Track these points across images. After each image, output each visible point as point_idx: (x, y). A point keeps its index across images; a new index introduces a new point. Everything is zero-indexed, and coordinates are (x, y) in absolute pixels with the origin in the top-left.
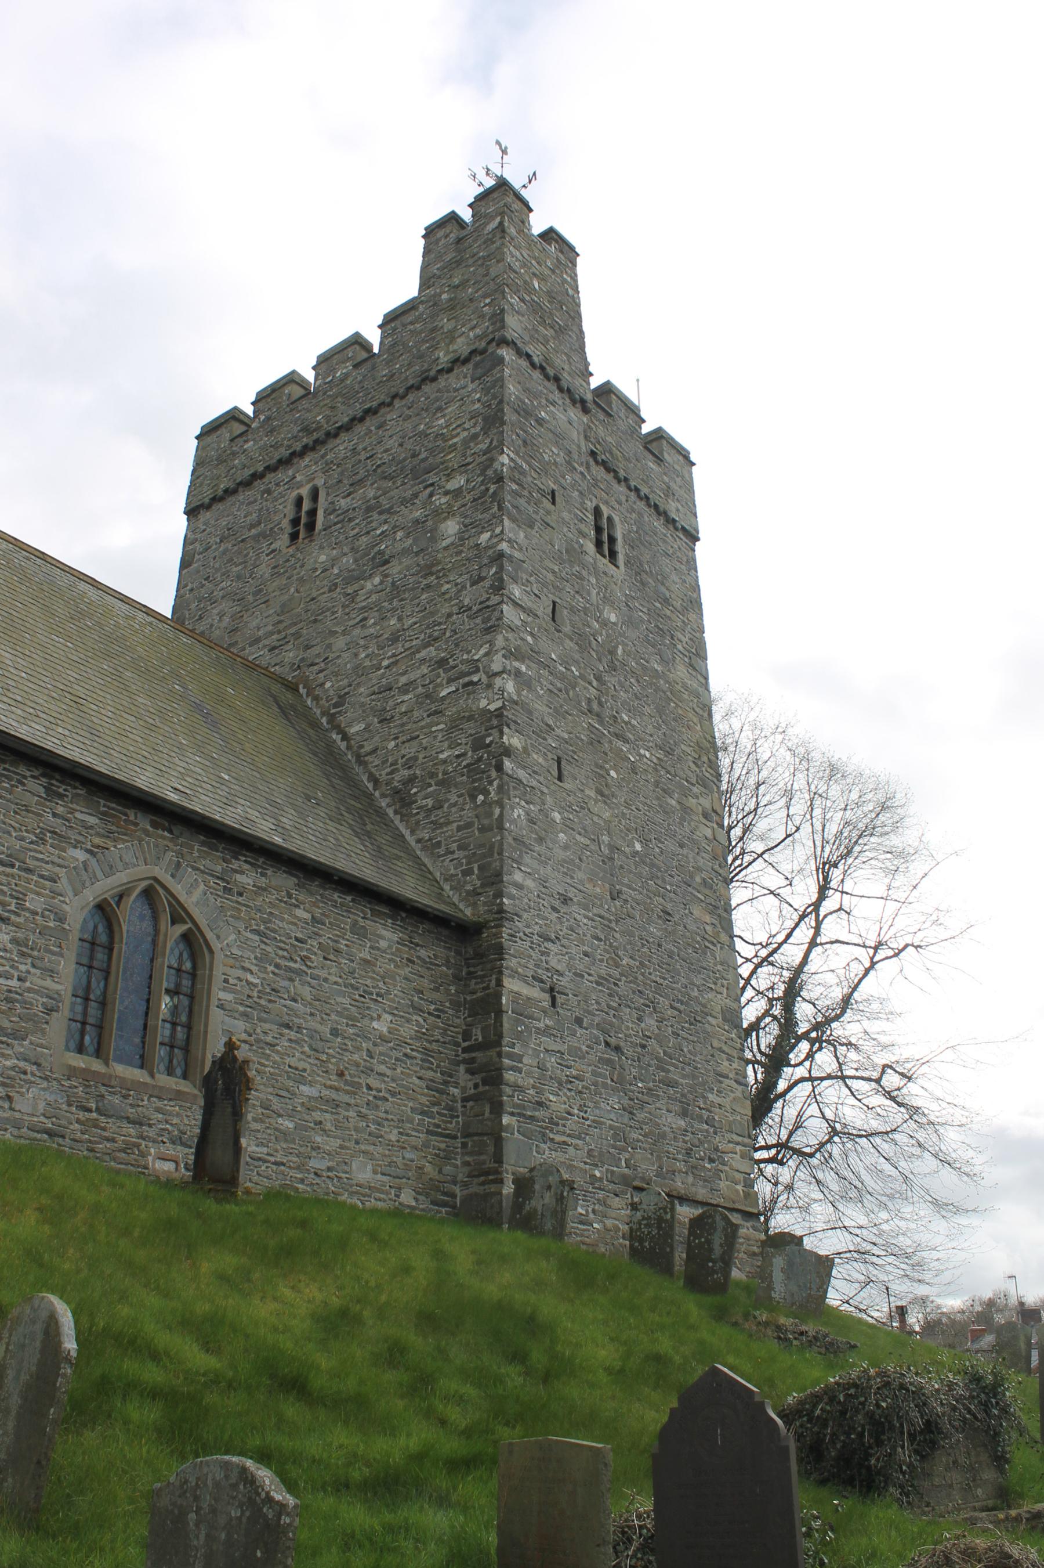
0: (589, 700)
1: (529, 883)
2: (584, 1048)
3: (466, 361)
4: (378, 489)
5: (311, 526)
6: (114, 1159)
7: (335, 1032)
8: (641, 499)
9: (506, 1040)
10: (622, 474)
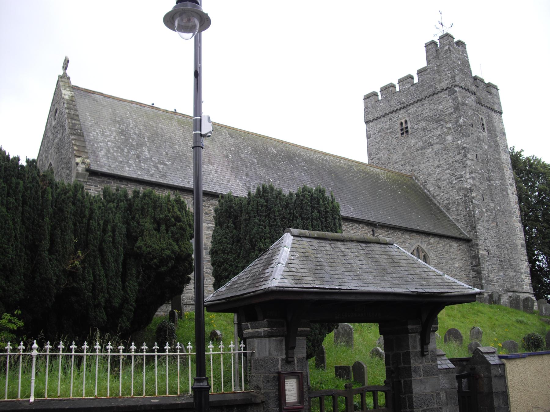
0: (487, 178)
1: (481, 228)
3: (446, 90)
5: (407, 132)
10: (483, 103)
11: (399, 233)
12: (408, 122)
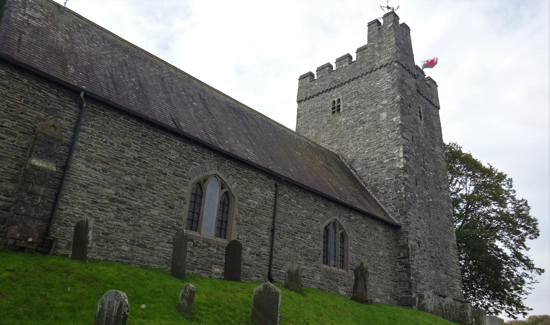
0: (421, 162)
1: (412, 214)
2: (426, 258)
3: (385, 66)
4: (359, 101)
5: (339, 110)
6: (333, 290)
7: (372, 256)
8: (426, 99)
9: (410, 256)
10: (422, 93)
11: (312, 198)
12: (341, 101)
